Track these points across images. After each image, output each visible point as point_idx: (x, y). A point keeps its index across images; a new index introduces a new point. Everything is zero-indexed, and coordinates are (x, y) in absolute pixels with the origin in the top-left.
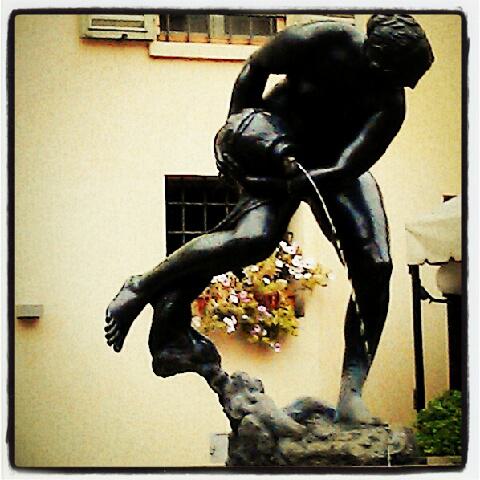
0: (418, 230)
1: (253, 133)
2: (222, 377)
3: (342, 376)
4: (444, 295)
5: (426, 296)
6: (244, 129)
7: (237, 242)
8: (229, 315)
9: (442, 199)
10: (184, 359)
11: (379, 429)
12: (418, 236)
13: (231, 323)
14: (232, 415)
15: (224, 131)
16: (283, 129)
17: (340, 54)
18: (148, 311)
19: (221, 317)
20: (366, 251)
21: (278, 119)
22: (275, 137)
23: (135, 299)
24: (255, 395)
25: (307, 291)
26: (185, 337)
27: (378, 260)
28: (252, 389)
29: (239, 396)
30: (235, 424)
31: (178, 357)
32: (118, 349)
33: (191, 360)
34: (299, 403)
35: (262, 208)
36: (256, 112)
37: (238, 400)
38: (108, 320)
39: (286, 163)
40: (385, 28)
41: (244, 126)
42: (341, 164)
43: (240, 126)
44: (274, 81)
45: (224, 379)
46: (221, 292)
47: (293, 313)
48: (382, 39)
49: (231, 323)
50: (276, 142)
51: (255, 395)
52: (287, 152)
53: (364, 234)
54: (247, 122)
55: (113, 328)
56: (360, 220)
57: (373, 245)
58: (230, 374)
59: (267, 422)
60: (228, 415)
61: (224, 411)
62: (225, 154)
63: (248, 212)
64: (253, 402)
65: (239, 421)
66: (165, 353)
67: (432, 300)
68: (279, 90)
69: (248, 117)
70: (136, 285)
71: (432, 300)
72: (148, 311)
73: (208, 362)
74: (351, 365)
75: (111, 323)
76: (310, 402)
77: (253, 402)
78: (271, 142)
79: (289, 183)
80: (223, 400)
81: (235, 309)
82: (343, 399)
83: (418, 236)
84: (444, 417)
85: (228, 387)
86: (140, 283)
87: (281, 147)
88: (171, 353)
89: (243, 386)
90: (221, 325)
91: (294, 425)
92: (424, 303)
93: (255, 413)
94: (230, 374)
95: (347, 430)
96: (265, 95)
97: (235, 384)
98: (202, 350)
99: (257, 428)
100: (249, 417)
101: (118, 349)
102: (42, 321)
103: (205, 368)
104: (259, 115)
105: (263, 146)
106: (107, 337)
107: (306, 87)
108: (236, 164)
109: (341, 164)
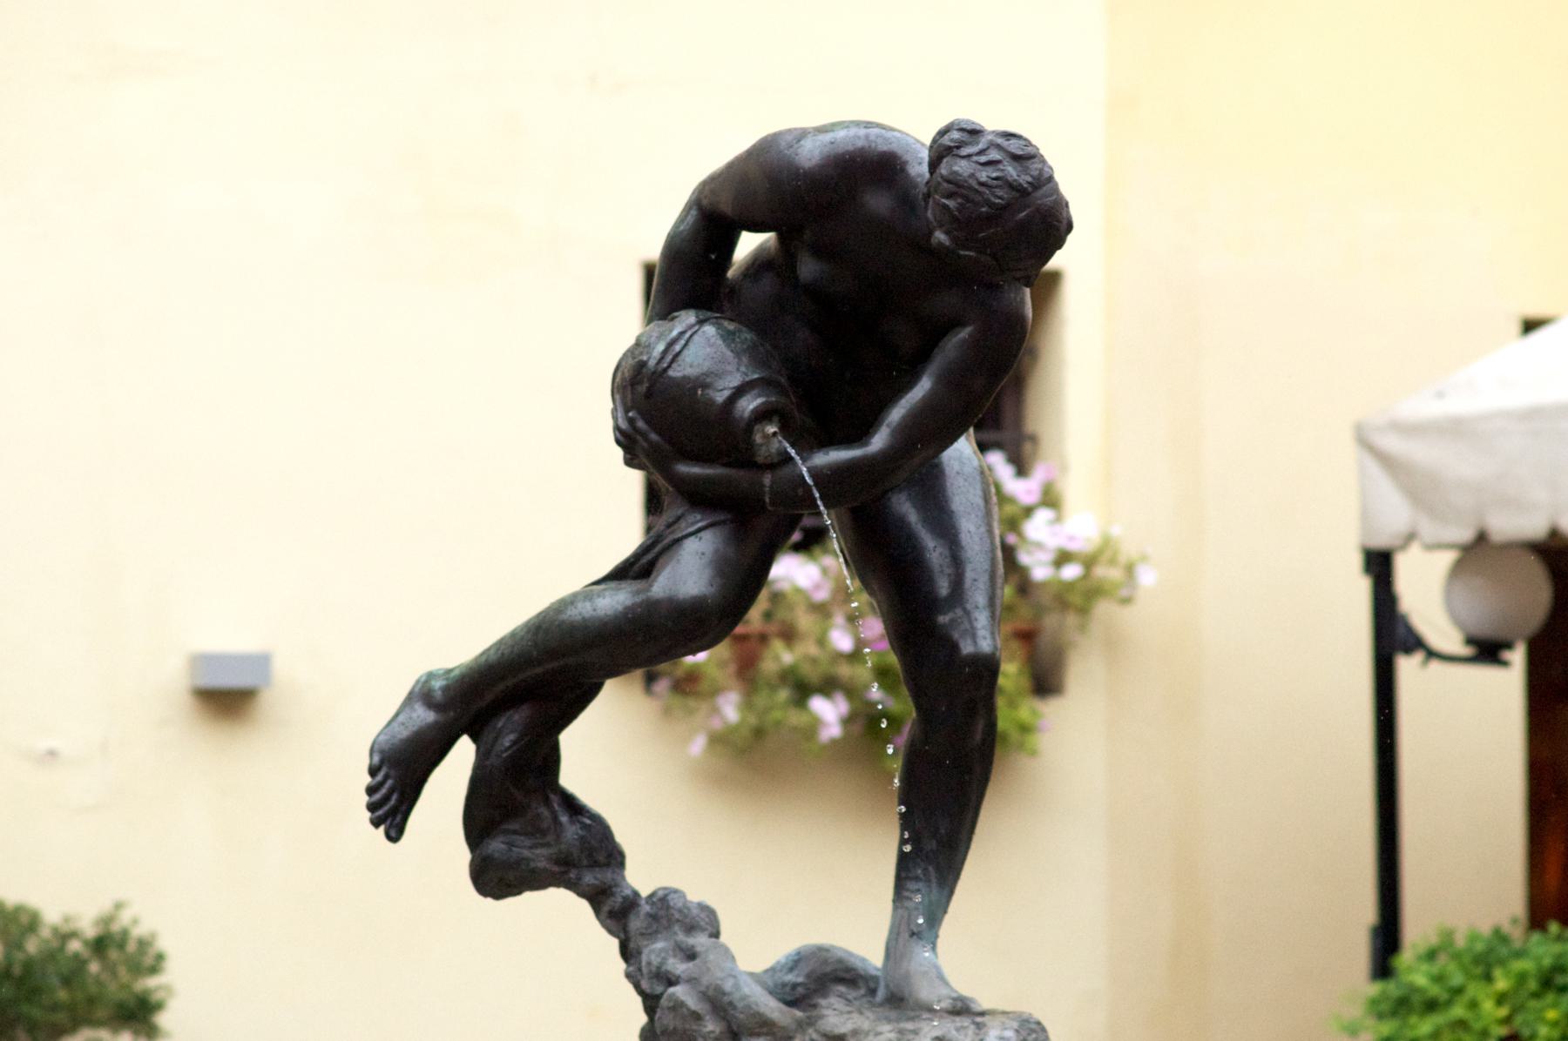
0: (1392, 444)
1: (689, 372)
2: (625, 898)
3: (894, 901)
4: (1470, 641)
5: (1414, 643)
6: (673, 361)
7: (652, 606)
8: (828, 687)
9: (1516, 327)
10: (540, 857)
11: (965, 1021)
12: (1386, 461)
13: (828, 712)
14: (645, 985)
15: (631, 361)
16: (758, 361)
17: (878, 203)
18: (463, 753)
19: (803, 690)
20: (944, 625)
21: (748, 335)
22: (735, 380)
23: (436, 723)
24: (700, 941)
25: (1071, 620)
26: (545, 812)
27: (967, 648)
28: (691, 928)
29: (659, 945)
30: (651, 1003)
31: (526, 853)
32: (395, 834)
33: (557, 862)
34: (797, 960)
35: (707, 536)
36: (701, 322)
37: (656, 951)
38: (373, 771)
39: (758, 438)
40: (963, 163)
41: (672, 354)
42: (879, 441)
43: (665, 352)
44: (748, 244)
45: (632, 902)
46: (805, 621)
47: (1026, 682)
48: (957, 186)
49: (828, 712)
50: (740, 392)
51: (700, 941)
52: (762, 415)
53: (943, 587)
54: (677, 348)
55: (384, 791)
56: (934, 551)
57: (959, 612)
58: (644, 893)
59: (719, 1003)
60: (637, 987)
61: (628, 976)
62: (630, 414)
63: (678, 541)
64: (691, 955)
65: (658, 997)
66: (496, 846)
67: (1432, 654)
68: (760, 264)
69: (682, 333)
70: (438, 695)
71: (1432, 654)
72: (463, 753)
73: (594, 864)
74: (907, 878)
75: (379, 777)
76: (825, 962)
77: (691, 955)
78: (727, 393)
79: (767, 479)
80: (626, 953)
81: (845, 671)
82: (893, 951)
83: (1386, 461)
84: (1431, 1006)
85: (636, 923)
86: (446, 689)
87: (749, 404)
88: (511, 845)
89: (671, 922)
90: (795, 718)
91: (771, 1007)
92: (1407, 667)
93: (692, 981)
94: (644, 893)
95: (889, 1021)
96: (730, 274)
97: (653, 917)
98: (582, 838)
99: (697, 1017)
100: (679, 991)
101: (395, 834)
102: (269, 701)
103: (589, 878)
104: (709, 330)
105: (711, 402)
106: (372, 807)
107: (808, 268)
108: (654, 437)
109: (879, 441)
